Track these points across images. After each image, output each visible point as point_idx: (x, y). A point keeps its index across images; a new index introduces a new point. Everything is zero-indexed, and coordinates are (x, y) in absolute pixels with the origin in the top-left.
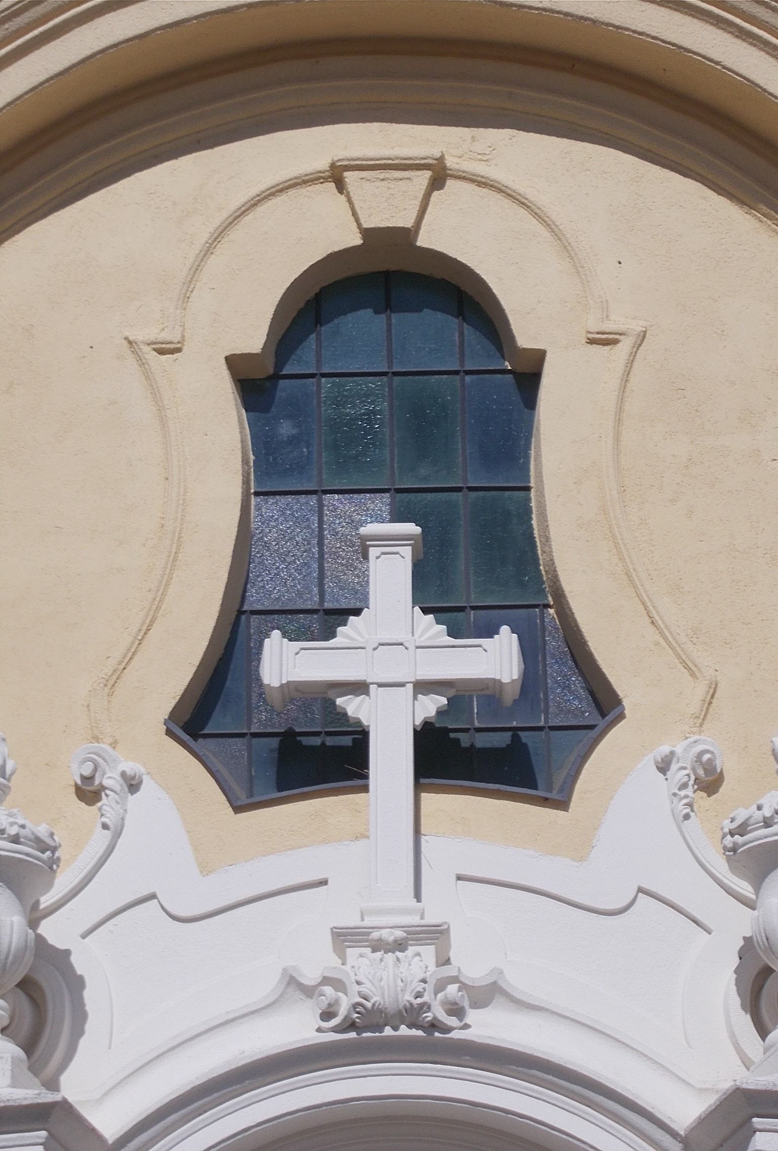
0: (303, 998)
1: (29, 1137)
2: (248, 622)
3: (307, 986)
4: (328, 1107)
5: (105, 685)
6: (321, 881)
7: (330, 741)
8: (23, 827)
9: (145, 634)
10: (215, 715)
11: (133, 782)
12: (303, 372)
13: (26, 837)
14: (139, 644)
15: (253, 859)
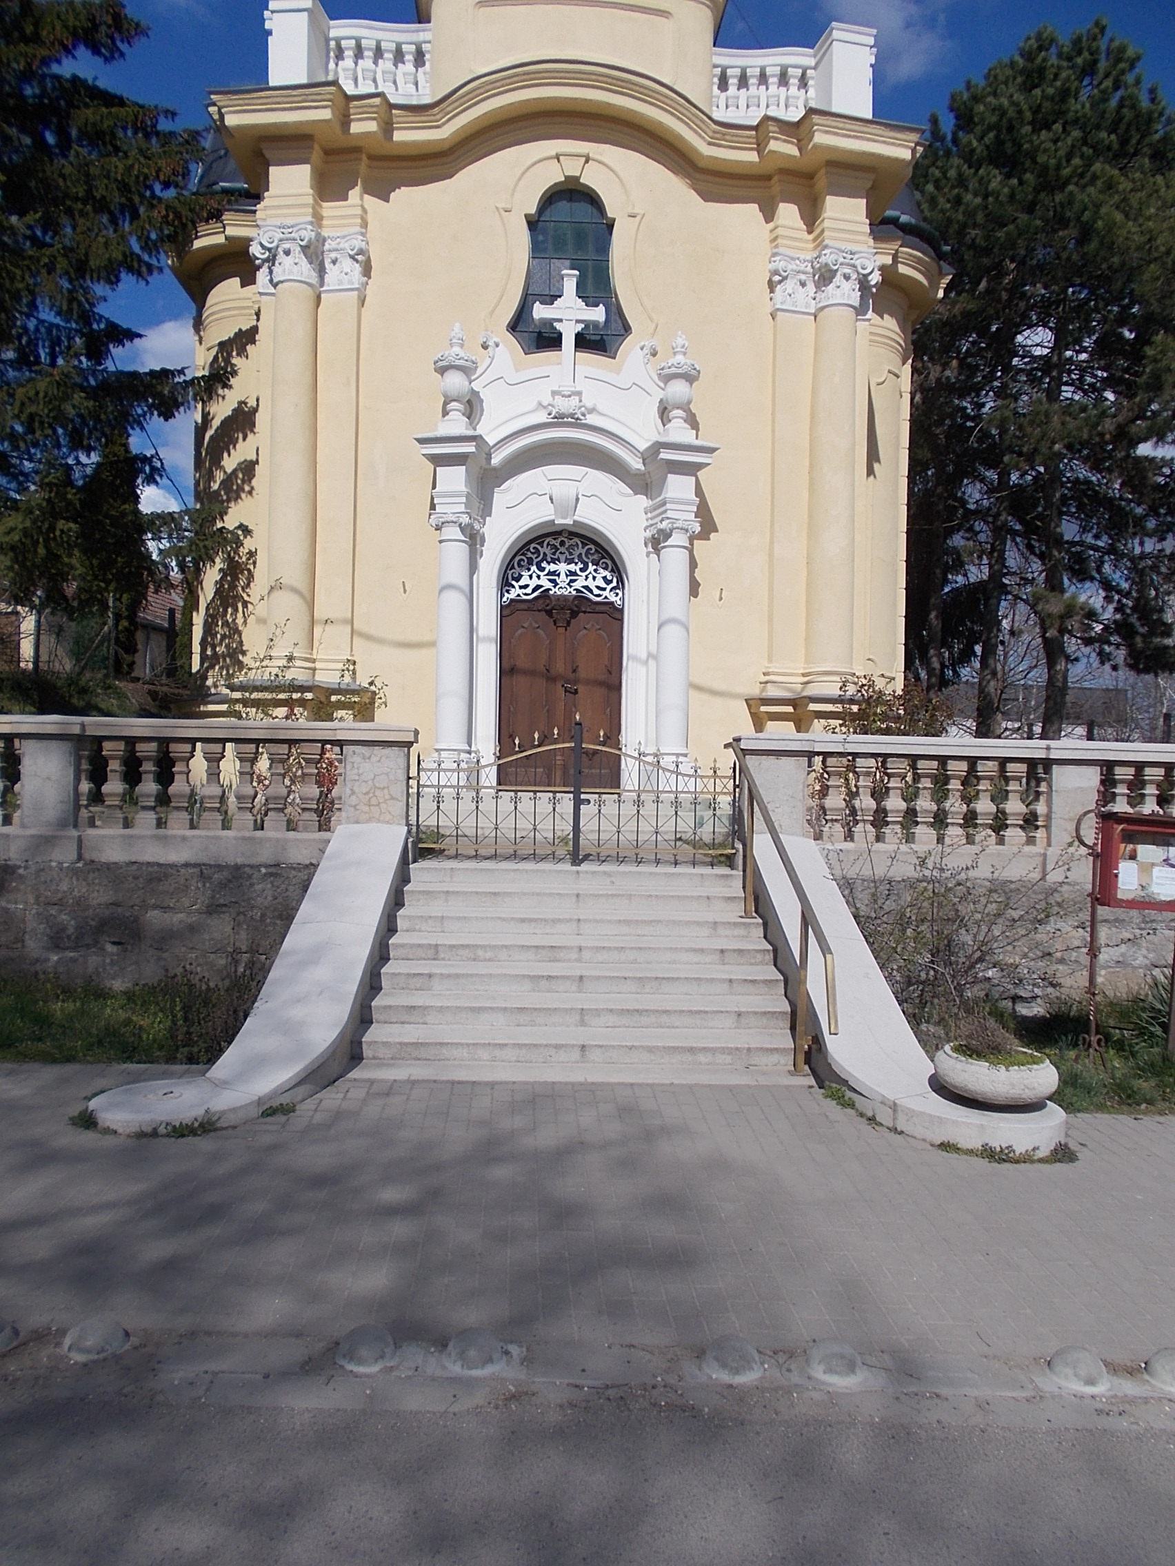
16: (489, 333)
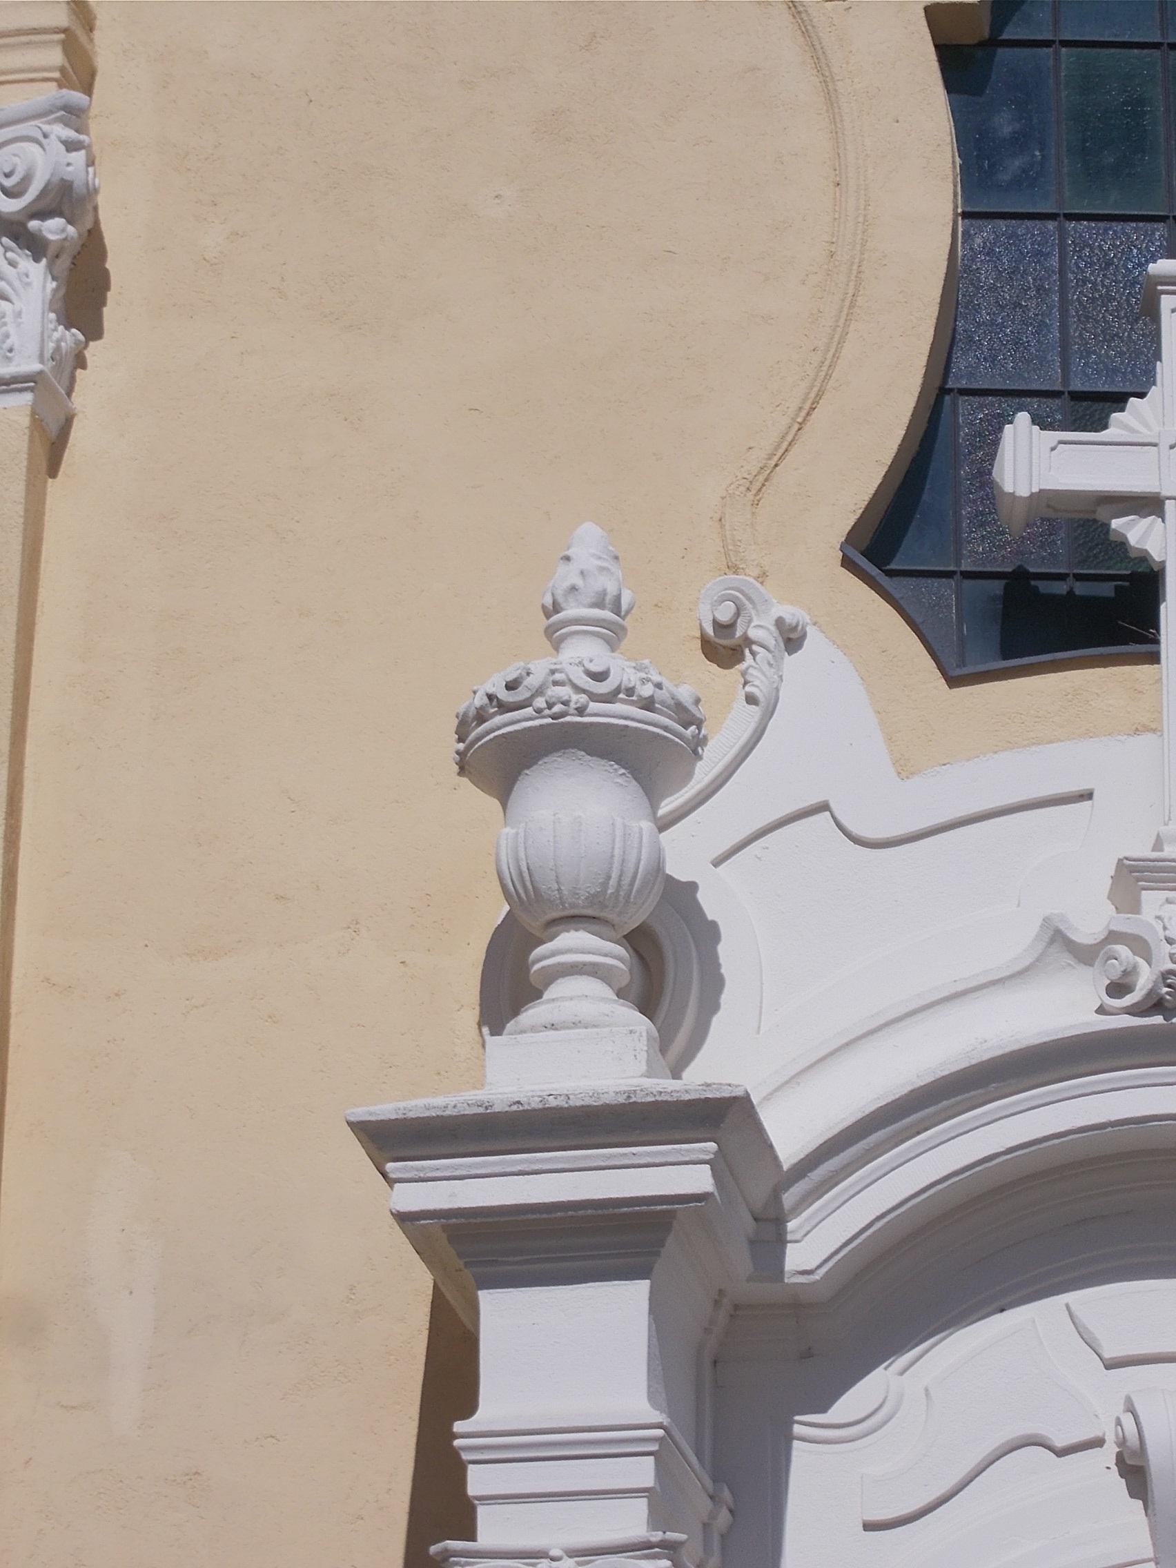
0: (1072, 963)
1: (688, 1150)
2: (955, 405)
3: (1079, 944)
4: (1115, 1129)
5: (748, 489)
6: (1082, 793)
7: (1080, 589)
8: (659, 686)
9: (808, 414)
10: (906, 542)
11: (792, 636)
12: (1032, 38)
13: (663, 703)
14: (799, 429)
15: (978, 757)
16: (747, 579)
